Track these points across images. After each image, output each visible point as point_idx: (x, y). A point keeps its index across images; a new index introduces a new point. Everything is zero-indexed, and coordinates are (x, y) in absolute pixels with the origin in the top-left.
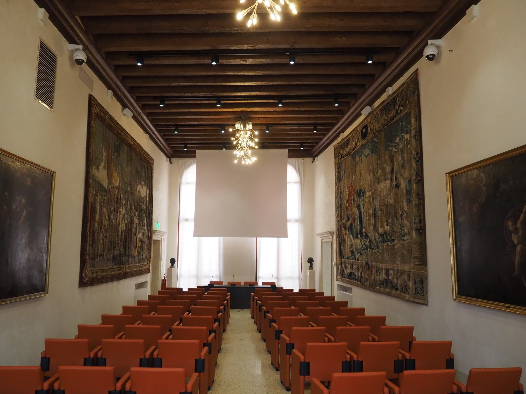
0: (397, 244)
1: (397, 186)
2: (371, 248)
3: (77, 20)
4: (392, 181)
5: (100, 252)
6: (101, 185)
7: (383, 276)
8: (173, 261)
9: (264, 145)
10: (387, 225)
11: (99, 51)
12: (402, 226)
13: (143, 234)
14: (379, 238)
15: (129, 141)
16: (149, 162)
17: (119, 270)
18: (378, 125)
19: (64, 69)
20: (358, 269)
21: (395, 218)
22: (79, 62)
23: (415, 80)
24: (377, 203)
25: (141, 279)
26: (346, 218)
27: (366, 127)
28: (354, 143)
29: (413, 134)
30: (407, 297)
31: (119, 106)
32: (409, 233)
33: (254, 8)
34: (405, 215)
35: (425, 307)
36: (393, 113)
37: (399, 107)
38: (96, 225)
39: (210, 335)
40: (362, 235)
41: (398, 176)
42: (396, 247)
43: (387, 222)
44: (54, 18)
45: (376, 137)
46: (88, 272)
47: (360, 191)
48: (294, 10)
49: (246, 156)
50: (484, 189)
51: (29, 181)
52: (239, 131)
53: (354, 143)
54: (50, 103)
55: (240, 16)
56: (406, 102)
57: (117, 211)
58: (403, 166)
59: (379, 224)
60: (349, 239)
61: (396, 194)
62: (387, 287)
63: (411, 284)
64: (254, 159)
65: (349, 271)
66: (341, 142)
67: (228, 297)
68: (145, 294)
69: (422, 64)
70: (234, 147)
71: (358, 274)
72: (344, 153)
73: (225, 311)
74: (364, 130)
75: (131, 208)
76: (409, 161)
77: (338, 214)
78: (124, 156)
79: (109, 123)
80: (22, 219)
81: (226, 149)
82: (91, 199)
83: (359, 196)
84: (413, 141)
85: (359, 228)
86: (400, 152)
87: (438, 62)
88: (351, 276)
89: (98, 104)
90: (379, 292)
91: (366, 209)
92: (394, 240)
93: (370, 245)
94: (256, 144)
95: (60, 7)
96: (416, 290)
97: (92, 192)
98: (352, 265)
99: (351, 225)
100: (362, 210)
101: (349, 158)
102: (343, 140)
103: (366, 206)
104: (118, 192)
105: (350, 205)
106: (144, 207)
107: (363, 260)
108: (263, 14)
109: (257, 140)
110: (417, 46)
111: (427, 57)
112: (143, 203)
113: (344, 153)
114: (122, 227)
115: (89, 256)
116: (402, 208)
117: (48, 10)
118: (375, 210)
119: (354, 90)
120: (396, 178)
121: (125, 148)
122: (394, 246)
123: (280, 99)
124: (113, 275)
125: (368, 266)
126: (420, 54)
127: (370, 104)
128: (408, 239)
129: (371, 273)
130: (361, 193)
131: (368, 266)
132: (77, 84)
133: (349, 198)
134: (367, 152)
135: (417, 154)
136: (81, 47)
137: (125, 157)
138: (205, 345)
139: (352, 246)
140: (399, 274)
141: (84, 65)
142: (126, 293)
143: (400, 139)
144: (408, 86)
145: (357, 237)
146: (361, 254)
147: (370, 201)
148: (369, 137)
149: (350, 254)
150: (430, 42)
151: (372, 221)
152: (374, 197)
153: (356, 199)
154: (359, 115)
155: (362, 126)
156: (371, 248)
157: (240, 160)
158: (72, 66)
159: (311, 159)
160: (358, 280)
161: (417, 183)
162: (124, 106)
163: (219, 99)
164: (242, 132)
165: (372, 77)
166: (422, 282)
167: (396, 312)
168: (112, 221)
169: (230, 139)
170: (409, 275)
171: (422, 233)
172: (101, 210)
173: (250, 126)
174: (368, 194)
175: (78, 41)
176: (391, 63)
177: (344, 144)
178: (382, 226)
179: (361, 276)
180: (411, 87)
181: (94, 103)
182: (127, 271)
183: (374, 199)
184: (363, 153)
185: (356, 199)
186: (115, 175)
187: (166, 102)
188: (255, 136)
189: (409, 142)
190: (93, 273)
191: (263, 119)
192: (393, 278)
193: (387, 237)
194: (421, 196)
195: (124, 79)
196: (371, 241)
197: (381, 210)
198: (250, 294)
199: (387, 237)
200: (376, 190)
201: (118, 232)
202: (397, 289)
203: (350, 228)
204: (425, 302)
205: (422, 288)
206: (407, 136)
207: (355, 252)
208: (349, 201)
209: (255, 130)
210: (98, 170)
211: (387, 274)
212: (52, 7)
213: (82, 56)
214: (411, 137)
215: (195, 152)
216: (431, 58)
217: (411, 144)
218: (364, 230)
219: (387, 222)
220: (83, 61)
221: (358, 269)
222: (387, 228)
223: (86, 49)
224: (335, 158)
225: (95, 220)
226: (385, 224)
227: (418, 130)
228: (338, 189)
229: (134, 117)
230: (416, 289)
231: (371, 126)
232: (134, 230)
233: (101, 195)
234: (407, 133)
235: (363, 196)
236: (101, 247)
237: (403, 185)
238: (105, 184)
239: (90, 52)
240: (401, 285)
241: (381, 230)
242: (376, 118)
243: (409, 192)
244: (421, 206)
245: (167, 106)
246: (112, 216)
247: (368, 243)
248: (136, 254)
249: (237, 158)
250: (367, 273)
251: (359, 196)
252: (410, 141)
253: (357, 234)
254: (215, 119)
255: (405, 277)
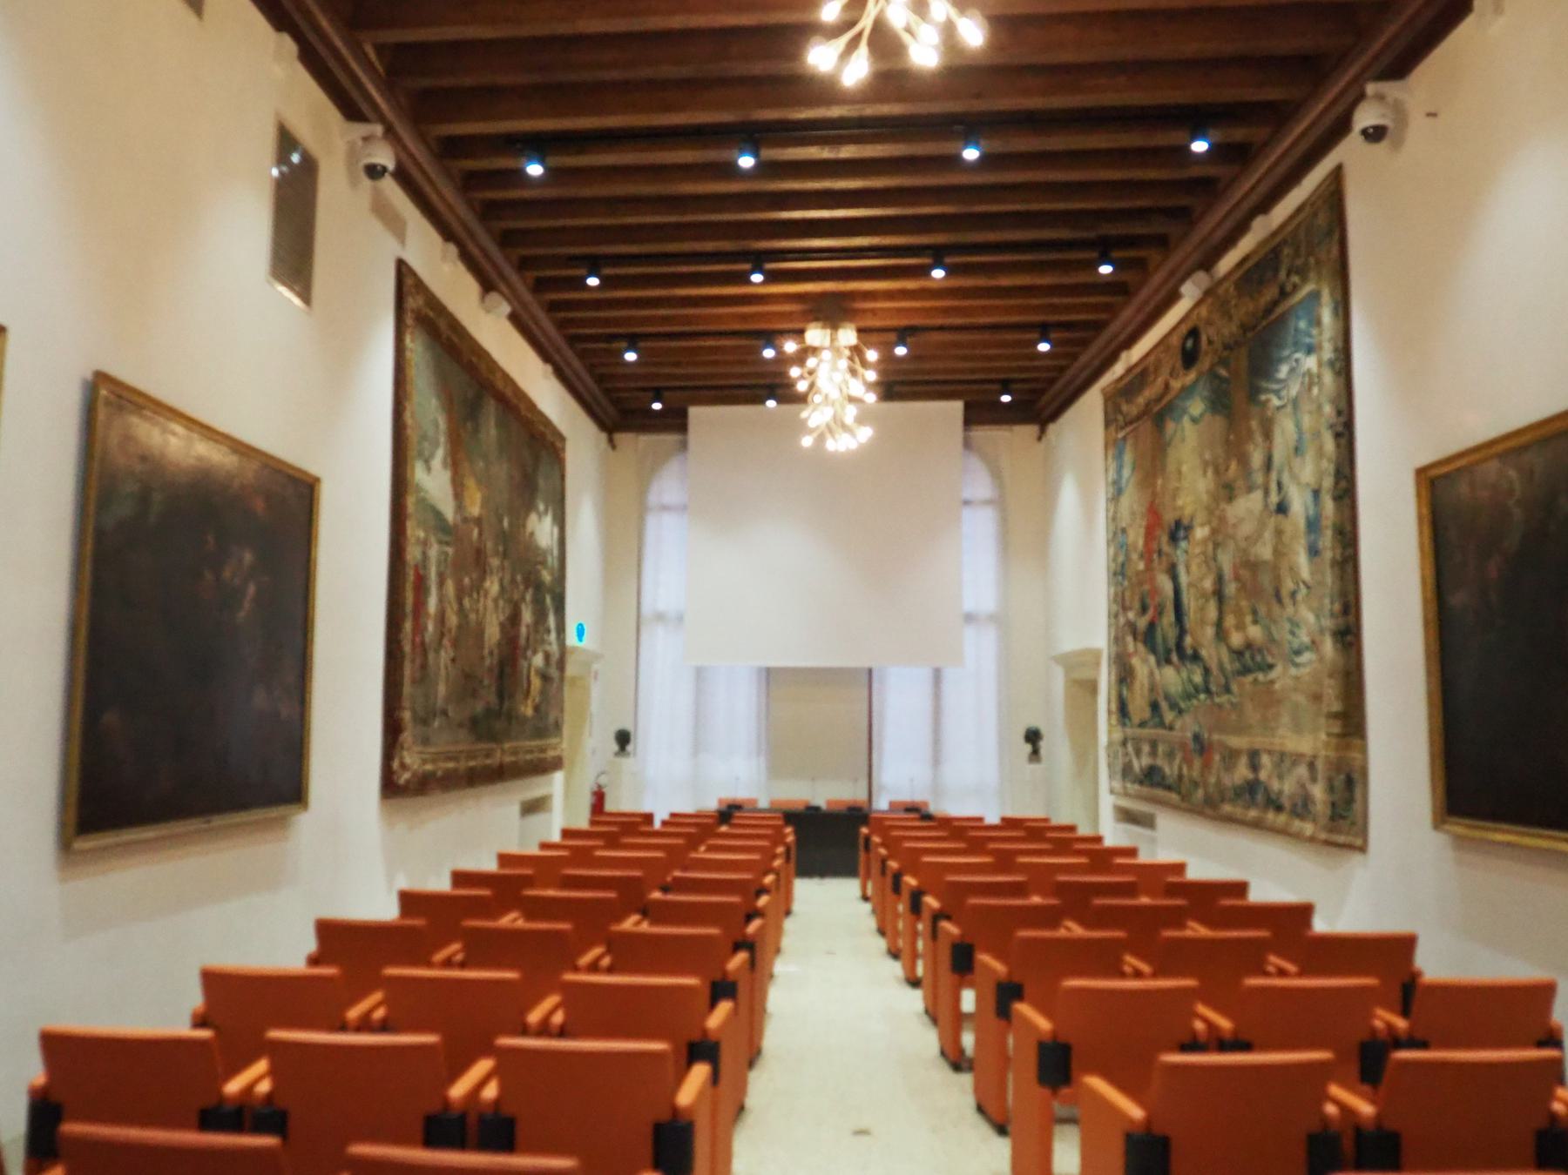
0: (1282, 676)
1: (1282, 508)
2: (1208, 691)
3: (365, 54)
4: (1267, 492)
5: (440, 703)
6: (438, 515)
7: (1242, 772)
8: (623, 739)
9: (894, 387)
10: (1255, 622)
11: (422, 138)
12: (1295, 624)
13: (547, 657)
14: (1231, 662)
15: (500, 384)
16: (553, 444)
17: (488, 756)
18: (1229, 329)
19: (341, 202)
20: (1170, 755)
21: (1274, 601)
22: (374, 172)
23: (1334, 196)
24: (1226, 560)
25: (534, 788)
26: (1137, 605)
27: (1194, 333)
28: (1160, 381)
29: (1328, 353)
30: (1308, 828)
31: (471, 285)
32: (1314, 645)
33: (860, 35)
34: (1303, 591)
35: (1357, 858)
36: (1270, 293)
37: (1288, 275)
38: (431, 627)
39: (713, 1005)
40: (1179, 652)
41: (1286, 478)
42: (1277, 686)
43: (1255, 612)
44: (311, 59)
45: (1223, 362)
46: (412, 759)
47: (1178, 523)
48: (974, 34)
49: (838, 424)
50: (1518, 514)
51: (259, 505)
52: (814, 351)
53: (1160, 381)
54: (306, 296)
55: (820, 57)
56: (1306, 264)
57: (478, 587)
58: (1298, 450)
59: (1230, 621)
60: (1143, 665)
61: (1279, 533)
62: (1250, 804)
63: (1318, 792)
64: (865, 433)
65: (1146, 761)
66: (1121, 378)
67: (777, 863)
68: (551, 826)
69: (1349, 152)
70: (802, 399)
71: (1170, 770)
72: (1131, 409)
73: (778, 888)
74: (1189, 344)
75: (513, 581)
76: (1317, 435)
77: (1116, 595)
78: (490, 431)
79: (449, 339)
80: (247, 605)
81: (780, 400)
82: (413, 554)
83: (1174, 538)
84: (1328, 378)
85: (1172, 634)
86: (1289, 409)
87: (1398, 144)
88: (1151, 777)
89: (420, 286)
90: (1230, 820)
91: (1194, 576)
92: (1271, 667)
93: (1206, 682)
94: (870, 386)
95: (324, 23)
96: (1342, 819)
97: (414, 531)
98: (1154, 745)
99: (1152, 626)
100: (1184, 579)
101: (1146, 426)
102: (1129, 370)
103: (1194, 568)
104: (480, 534)
105: (1149, 568)
106: (546, 577)
107: (1186, 727)
108: (884, 42)
109: (871, 376)
110: (1334, 102)
111: (1364, 132)
112: (544, 563)
113: (1131, 409)
114: (493, 633)
115: (414, 711)
116: (1293, 570)
117: (298, 37)
118: (1220, 580)
119: (1157, 227)
120: (1280, 485)
121: (490, 409)
122: (1272, 682)
123: (938, 255)
124: (472, 769)
125: (1202, 746)
126: (1341, 127)
127: (1207, 264)
128: (1310, 662)
129: (1207, 765)
130: (1179, 531)
131: (1202, 746)
132: (378, 237)
133: (1146, 543)
134: (1196, 407)
135: (1339, 413)
136: (378, 129)
137: (493, 432)
138: (737, 947)
139: (1152, 689)
140: (1287, 763)
141: (389, 186)
142: (483, 833)
143: (1292, 370)
144: (1315, 214)
145: (1168, 661)
146: (1181, 712)
147: (1204, 553)
148: (1205, 363)
149: (1147, 714)
150: (1371, 88)
151: (1212, 612)
152: (1217, 539)
153: (1166, 548)
154: (1173, 297)
155: (1184, 329)
156: (1208, 691)
157: (821, 439)
158: (354, 183)
159: (1033, 429)
160: (1169, 788)
161: (1337, 499)
162: (487, 286)
163: (758, 260)
164: (826, 355)
165: (1206, 187)
166: (1350, 783)
167: (1272, 872)
168: (466, 616)
169: (785, 375)
170: (1312, 766)
171: (1350, 644)
172: (441, 584)
173: (848, 336)
174: (1200, 533)
175: (365, 108)
176: (1266, 145)
177: (1131, 383)
178: (1240, 627)
179: (1180, 777)
180: (1322, 220)
181: (409, 281)
182: (508, 759)
183: (1216, 545)
184: (1185, 411)
185: (1166, 548)
186: (471, 483)
187: (607, 271)
188: (865, 364)
189: (1312, 380)
190: (425, 762)
191: (887, 313)
192: (1270, 777)
193: (1253, 658)
194: (1348, 536)
195: (488, 211)
196: (1207, 672)
197: (1237, 578)
198: (857, 833)
199: (1253, 658)
200: (1223, 519)
201: (482, 648)
202: (1279, 808)
203: (1148, 637)
204: (1359, 842)
205: (1350, 801)
206: (1310, 363)
207: (1164, 705)
208: (1147, 555)
209: (869, 345)
210: (429, 469)
211: (1255, 767)
212: (304, 26)
213: (384, 157)
214: (1320, 364)
215: (683, 415)
216: (1375, 134)
217: (1320, 384)
218: (1188, 640)
219: (1255, 612)
220: (384, 169)
221: (1170, 755)
222: (1255, 632)
223: (390, 133)
224: (1107, 424)
225: (427, 614)
226: (1249, 619)
227: (1340, 344)
228: (1114, 519)
229: (514, 318)
230: (1333, 804)
231: (1211, 331)
232: (522, 641)
233: (440, 542)
234: (1310, 350)
235: (1186, 538)
236: (442, 689)
237: (1299, 504)
238: (449, 512)
239: (405, 148)
240: (1291, 797)
241: (1236, 639)
242: (1224, 308)
243: (1313, 525)
244: (1349, 569)
245: (606, 282)
246: (467, 602)
247: (1198, 678)
248: (529, 712)
249: (811, 431)
250: (1197, 763)
251: (1174, 538)
252: (1319, 376)
253: (1168, 652)
254: (744, 318)
255: (1302, 771)
